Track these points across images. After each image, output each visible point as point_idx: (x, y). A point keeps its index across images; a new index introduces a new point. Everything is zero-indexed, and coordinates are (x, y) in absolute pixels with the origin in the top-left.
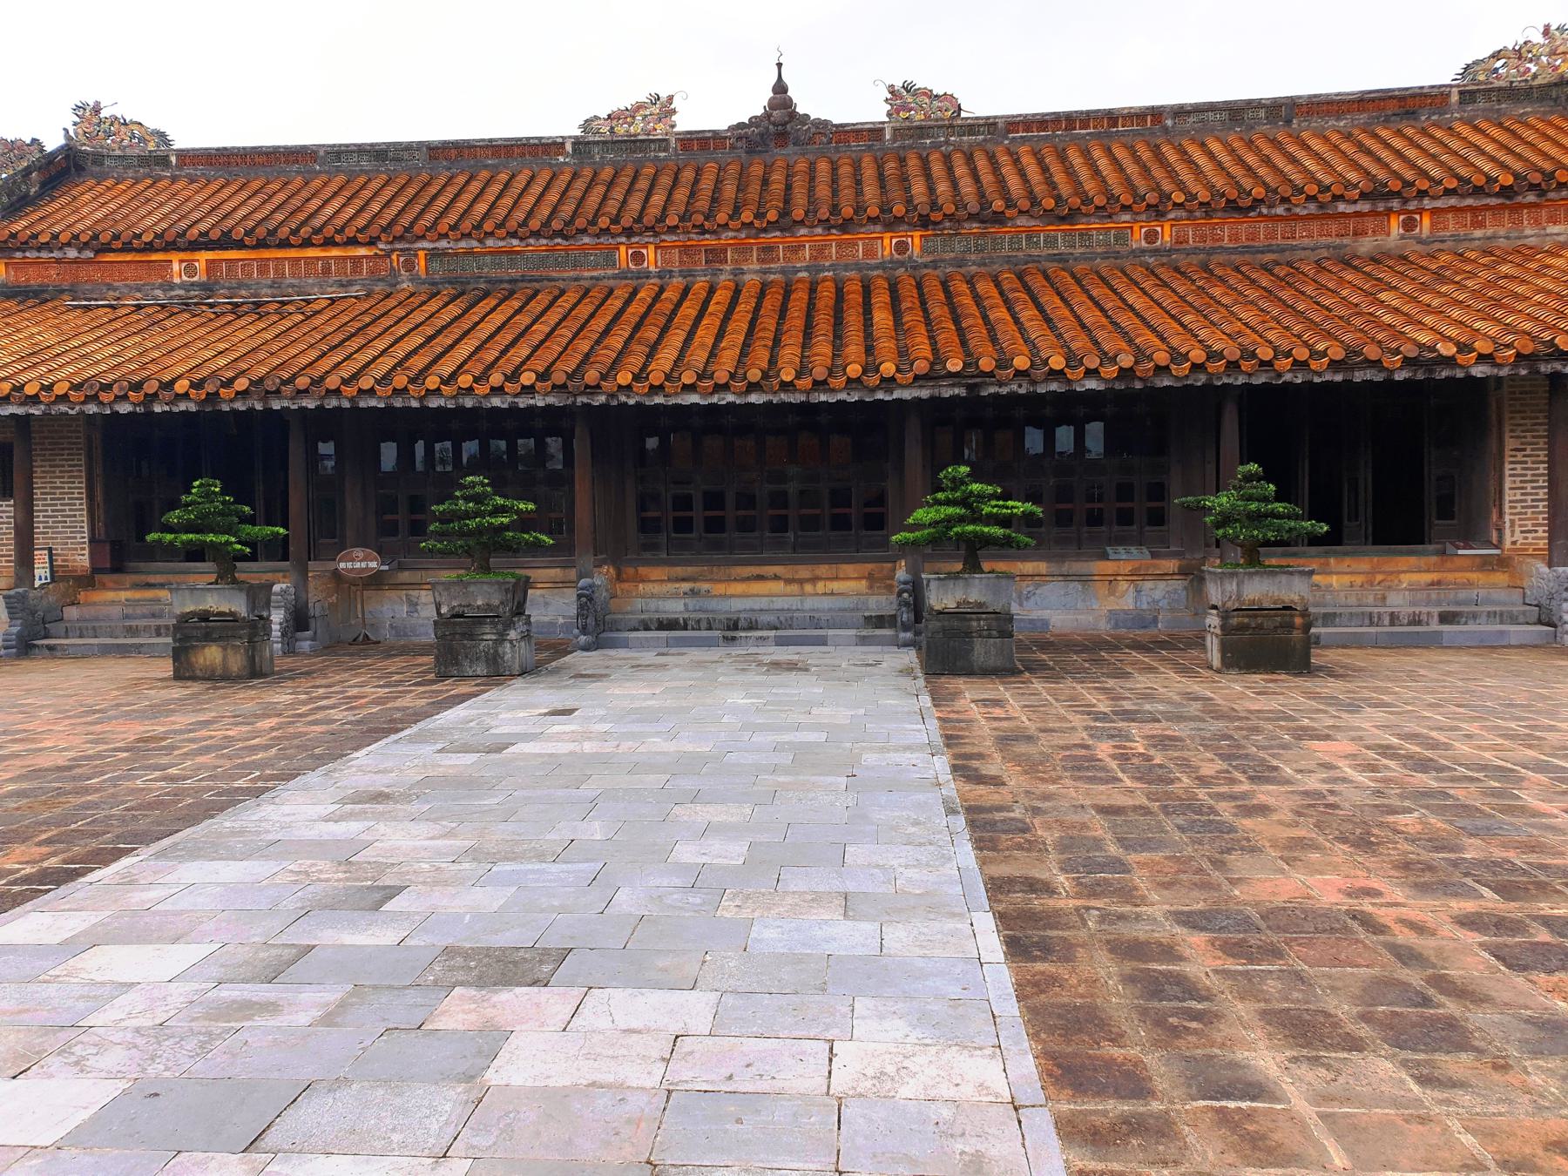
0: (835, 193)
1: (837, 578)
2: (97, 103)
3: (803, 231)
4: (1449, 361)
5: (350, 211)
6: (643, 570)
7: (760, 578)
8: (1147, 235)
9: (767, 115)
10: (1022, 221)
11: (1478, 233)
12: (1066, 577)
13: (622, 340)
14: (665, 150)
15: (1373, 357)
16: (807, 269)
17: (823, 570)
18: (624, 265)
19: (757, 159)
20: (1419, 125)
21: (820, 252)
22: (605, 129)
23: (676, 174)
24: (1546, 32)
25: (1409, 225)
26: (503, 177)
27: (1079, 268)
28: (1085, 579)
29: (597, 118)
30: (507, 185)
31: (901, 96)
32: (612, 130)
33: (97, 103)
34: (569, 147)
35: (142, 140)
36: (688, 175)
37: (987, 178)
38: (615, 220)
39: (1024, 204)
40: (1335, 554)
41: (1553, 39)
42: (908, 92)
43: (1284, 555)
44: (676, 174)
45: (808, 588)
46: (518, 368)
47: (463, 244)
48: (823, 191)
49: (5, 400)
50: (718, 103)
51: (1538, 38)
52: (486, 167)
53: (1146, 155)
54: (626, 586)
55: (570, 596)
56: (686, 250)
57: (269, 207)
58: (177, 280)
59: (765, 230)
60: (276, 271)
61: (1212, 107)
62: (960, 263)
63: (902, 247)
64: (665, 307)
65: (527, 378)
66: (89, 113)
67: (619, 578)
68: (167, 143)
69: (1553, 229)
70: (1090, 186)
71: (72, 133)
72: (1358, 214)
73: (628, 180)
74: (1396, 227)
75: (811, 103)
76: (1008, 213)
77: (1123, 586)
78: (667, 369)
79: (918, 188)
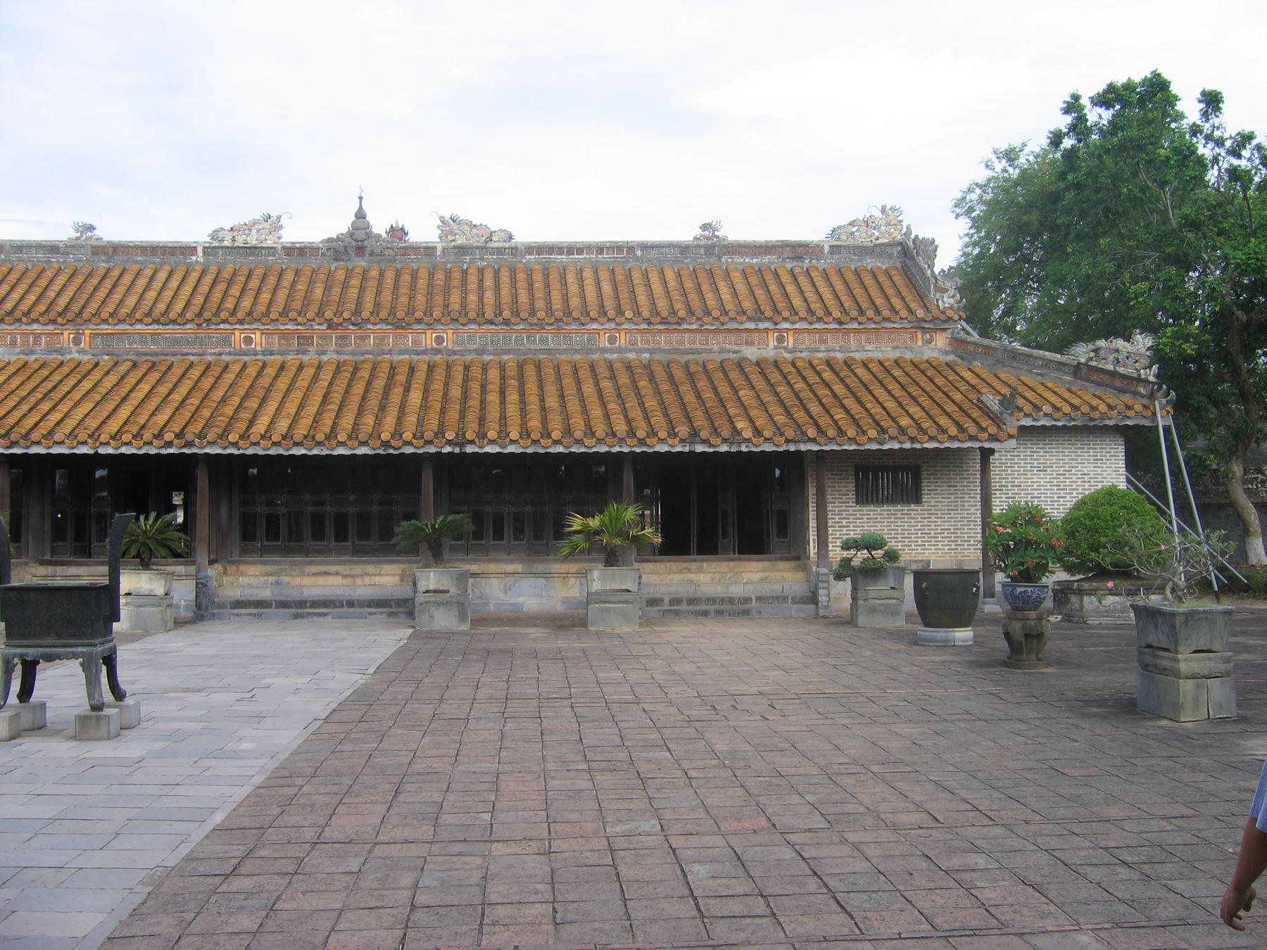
1: (379, 575)
5: (32, 298)
7: (326, 573)
12: (536, 575)
13: (233, 409)
14: (273, 255)
17: (370, 568)
18: (238, 347)
21: (381, 340)
22: (229, 238)
23: (281, 275)
24: (883, 211)
25: (780, 340)
26: (148, 272)
28: (546, 575)
29: (222, 229)
30: (152, 278)
31: (449, 225)
32: (233, 240)
34: (200, 251)
36: (289, 276)
38: (233, 313)
40: (707, 560)
44: (281, 275)
45: (359, 581)
46: (162, 429)
47: (120, 327)
48: (387, 297)
51: (878, 214)
52: (136, 262)
54: (230, 579)
55: (191, 584)
56: (284, 336)
61: (671, 245)
63: (439, 340)
64: (265, 381)
65: (169, 436)
67: (225, 572)
74: (772, 343)
75: (379, 226)
77: (572, 580)
78: (262, 432)
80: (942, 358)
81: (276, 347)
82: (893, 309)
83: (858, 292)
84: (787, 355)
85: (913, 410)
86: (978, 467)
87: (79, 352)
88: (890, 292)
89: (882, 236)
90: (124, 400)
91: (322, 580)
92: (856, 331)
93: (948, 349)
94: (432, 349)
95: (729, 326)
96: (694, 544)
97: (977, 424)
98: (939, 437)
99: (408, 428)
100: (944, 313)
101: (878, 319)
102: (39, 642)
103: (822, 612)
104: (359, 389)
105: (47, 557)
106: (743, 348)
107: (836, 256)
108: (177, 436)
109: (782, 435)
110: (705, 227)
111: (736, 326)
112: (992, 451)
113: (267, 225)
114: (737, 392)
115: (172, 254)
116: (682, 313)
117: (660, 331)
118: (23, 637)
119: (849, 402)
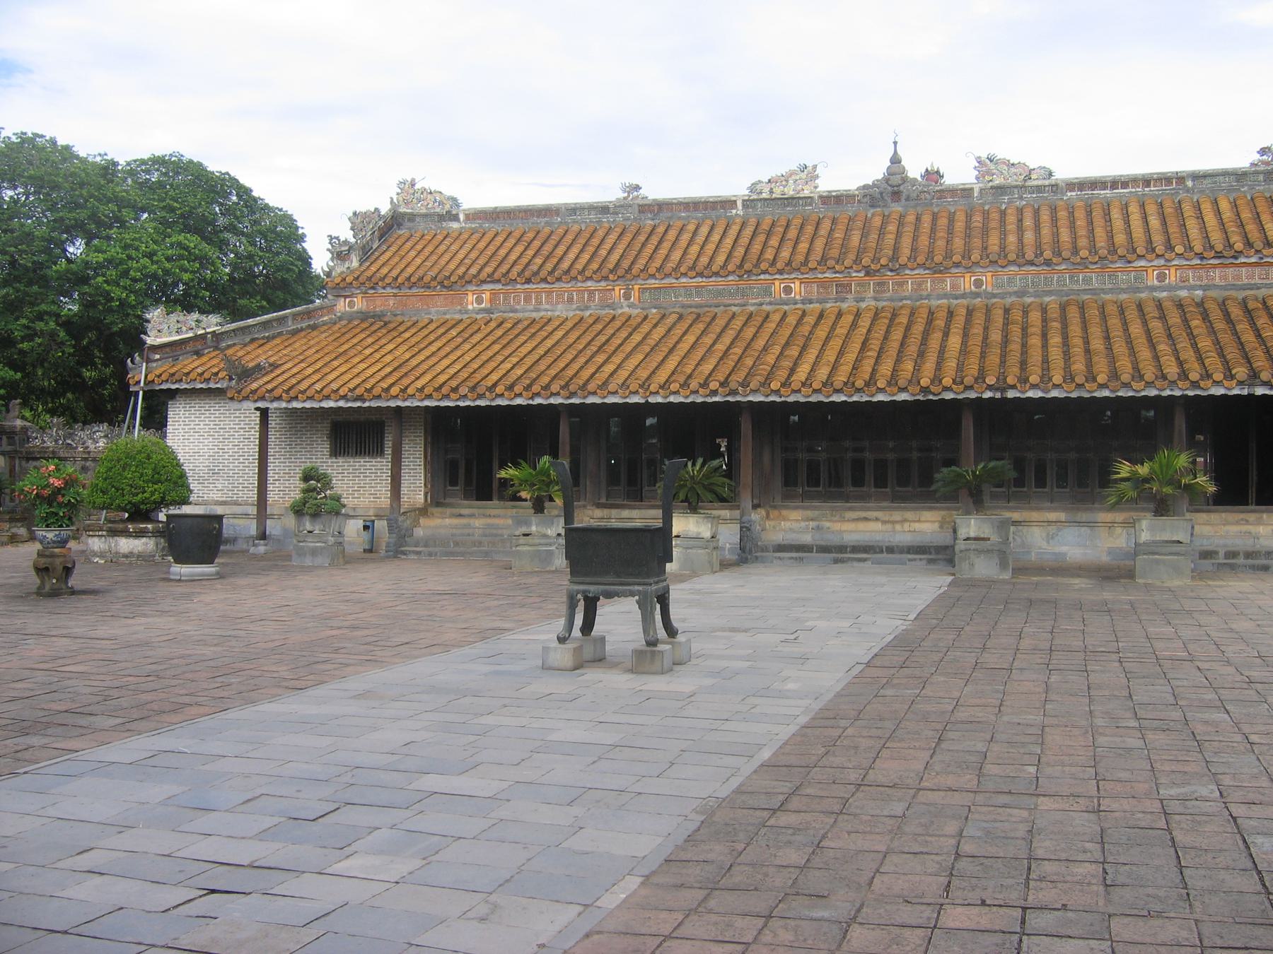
1: (919, 521)
2: (413, 180)
6: (784, 512)
7: (866, 519)
9: (886, 180)
12: (1079, 523)
14: (811, 205)
17: (909, 515)
23: (818, 224)
26: (691, 227)
28: (1091, 524)
30: (695, 233)
31: (986, 165)
32: (771, 192)
33: (413, 180)
34: (739, 204)
35: (441, 203)
36: (826, 225)
37: (1046, 231)
38: (773, 263)
42: (991, 161)
43: (862, 509)
44: (818, 224)
45: (898, 527)
46: (707, 378)
47: (667, 281)
48: (924, 241)
50: (849, 171)
52: (680, 218)
54: (772, 523)
56: (823, 284)
57: (530, 252)
58: (470, 307)
60: (537, 299)
63: (978, 283)
64: (805, 329)
66: (408, 187)
67: (768, 517)
68: (458, 206)
73: (782, 230)
77: (1119, 530)
78: (803, 379)
81: (815, 296)
90: (671, 351)
91: (861, 526)
94: (971, 293)
105: (603, 500)
113: (803, 175)
116: (1239, 246)
117: (1215, 267)
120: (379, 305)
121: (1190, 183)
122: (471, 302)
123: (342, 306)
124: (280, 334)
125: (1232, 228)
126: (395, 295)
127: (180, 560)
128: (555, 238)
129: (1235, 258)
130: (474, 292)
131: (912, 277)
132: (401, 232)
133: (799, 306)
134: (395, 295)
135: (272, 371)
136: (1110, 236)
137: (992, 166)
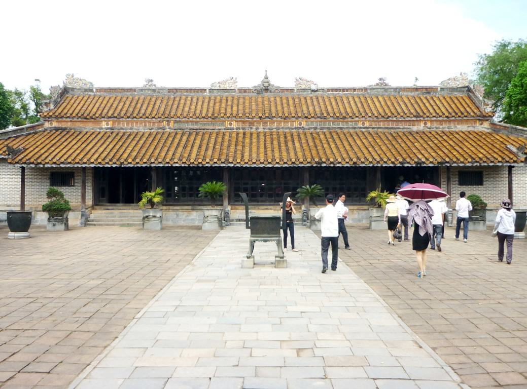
0: (283, 108)
3: (275, 119)
4: (424, 163)
8: (362, 123)
10: (331, 119)
11: (441, 127)
15: (408, 161)
16: (276, 128)
19: (260, 96)
20: (431, 96)
24: (461, 74)
25: (425, 124)
27: (345, 131)
29: (215, 83)
31: (299, 80)
32: (220, 87)
34: (208, 91)
37: (322, 106)
39: (332, 115)
41: (463, 76)
49: (1, 154)
50: (251, 81)
51: (459, 76)
53: (363, 100)
58: (103, 127)
59: (265, 118)
60: (131, 125)
62: (315, 128)
63: (300, 124)
69: (458, 127)
70: (349, 110)
71: (65, 82)
72: (413, 121)
74: (422, 124)
76: (328, 117)
77: (355, 212)
79: (305, 108)
80: (487, 131)
81: (241, 127)
82: (468, 112)
83: (453, 106)
84: (428, 130)
85: (482, 151)
86: (507, 173)
87: (169, 128)
88: (466, 106)
89: (460, 84)
90: (192, 146)
91: (267, 211)
92: (453, 121)
93: (489, 127)
94: (298, 127)
95: (407, 119)
96: (135, 201)
97: (509, 157)
98: (464, 162)
99: (296, 155)
100: (487, 114)
101: (462, 116)
102: (262, 236)
103: (450, 225)
104: (155, 143)
105: (165, 203)
106: (411, 127)
107: (443, 92)
108: (133, 160)
109: (390, 160)
110: (380, 79)
111: (409, 119)
112: (514, 167)
113: (232, 81)
114: (413, 144)
115: (198, 92)
116: (389, 114)
117: (381, 121)
118: (257, 234)
119: (457, 148)
120: (63, 125)
121: (369, 91)
122: (104, 125)
123: (47, 125)
124: (20, 136)
125: (386, 108)
126: (71, 121)
127: (13, 231)
128: (141, 101)
129: (388, 118)
130: (105, 121)
131: (277, 121)
132: (68, 95)
133: (235, 130)
134: (71, 121)
135: (25, 151)
136: (345, 109)
137: (301, 81)
